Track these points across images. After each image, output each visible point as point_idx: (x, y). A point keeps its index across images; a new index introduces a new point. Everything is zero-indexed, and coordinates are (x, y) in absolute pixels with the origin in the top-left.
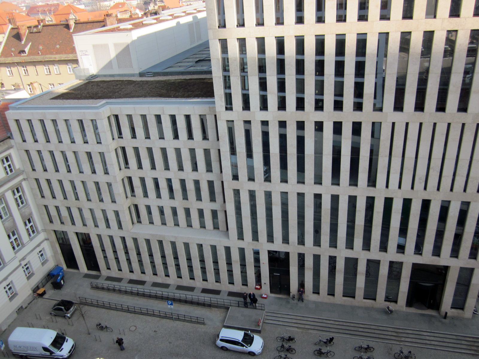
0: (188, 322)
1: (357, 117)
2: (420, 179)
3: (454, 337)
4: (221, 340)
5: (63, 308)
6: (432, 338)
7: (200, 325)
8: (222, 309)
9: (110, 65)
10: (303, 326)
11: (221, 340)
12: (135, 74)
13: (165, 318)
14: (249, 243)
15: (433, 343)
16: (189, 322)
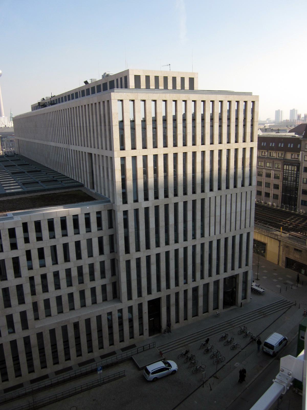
0: (112, 381)
1: (40, 244)
4: (153, 373)
7: (122, 378)
11: (153, 373)
14: (136, 300)
15: (246, 320)
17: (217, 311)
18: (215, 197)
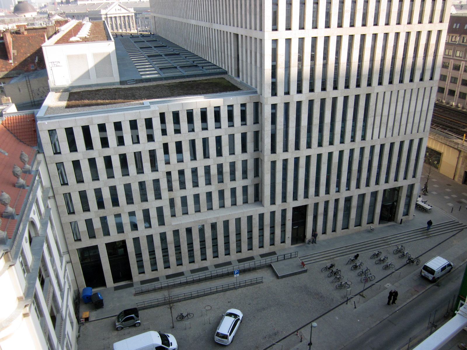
2: (390, 129)
3: (413, 232)
5: (133, 315)
6: (403, 237)
8: (265, 269)
9: (87, 74)
10: (328, 258)
12: (115, 82)
13: (228, 290)
16: (250, 286)
17: (372, 226)
18: (385, 92)
